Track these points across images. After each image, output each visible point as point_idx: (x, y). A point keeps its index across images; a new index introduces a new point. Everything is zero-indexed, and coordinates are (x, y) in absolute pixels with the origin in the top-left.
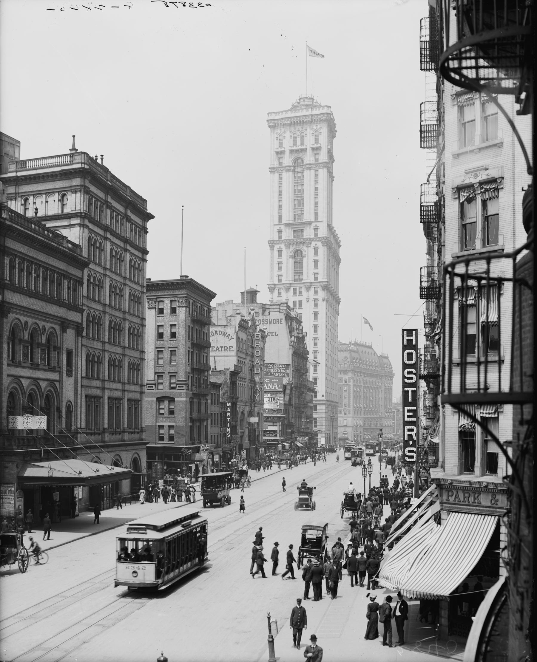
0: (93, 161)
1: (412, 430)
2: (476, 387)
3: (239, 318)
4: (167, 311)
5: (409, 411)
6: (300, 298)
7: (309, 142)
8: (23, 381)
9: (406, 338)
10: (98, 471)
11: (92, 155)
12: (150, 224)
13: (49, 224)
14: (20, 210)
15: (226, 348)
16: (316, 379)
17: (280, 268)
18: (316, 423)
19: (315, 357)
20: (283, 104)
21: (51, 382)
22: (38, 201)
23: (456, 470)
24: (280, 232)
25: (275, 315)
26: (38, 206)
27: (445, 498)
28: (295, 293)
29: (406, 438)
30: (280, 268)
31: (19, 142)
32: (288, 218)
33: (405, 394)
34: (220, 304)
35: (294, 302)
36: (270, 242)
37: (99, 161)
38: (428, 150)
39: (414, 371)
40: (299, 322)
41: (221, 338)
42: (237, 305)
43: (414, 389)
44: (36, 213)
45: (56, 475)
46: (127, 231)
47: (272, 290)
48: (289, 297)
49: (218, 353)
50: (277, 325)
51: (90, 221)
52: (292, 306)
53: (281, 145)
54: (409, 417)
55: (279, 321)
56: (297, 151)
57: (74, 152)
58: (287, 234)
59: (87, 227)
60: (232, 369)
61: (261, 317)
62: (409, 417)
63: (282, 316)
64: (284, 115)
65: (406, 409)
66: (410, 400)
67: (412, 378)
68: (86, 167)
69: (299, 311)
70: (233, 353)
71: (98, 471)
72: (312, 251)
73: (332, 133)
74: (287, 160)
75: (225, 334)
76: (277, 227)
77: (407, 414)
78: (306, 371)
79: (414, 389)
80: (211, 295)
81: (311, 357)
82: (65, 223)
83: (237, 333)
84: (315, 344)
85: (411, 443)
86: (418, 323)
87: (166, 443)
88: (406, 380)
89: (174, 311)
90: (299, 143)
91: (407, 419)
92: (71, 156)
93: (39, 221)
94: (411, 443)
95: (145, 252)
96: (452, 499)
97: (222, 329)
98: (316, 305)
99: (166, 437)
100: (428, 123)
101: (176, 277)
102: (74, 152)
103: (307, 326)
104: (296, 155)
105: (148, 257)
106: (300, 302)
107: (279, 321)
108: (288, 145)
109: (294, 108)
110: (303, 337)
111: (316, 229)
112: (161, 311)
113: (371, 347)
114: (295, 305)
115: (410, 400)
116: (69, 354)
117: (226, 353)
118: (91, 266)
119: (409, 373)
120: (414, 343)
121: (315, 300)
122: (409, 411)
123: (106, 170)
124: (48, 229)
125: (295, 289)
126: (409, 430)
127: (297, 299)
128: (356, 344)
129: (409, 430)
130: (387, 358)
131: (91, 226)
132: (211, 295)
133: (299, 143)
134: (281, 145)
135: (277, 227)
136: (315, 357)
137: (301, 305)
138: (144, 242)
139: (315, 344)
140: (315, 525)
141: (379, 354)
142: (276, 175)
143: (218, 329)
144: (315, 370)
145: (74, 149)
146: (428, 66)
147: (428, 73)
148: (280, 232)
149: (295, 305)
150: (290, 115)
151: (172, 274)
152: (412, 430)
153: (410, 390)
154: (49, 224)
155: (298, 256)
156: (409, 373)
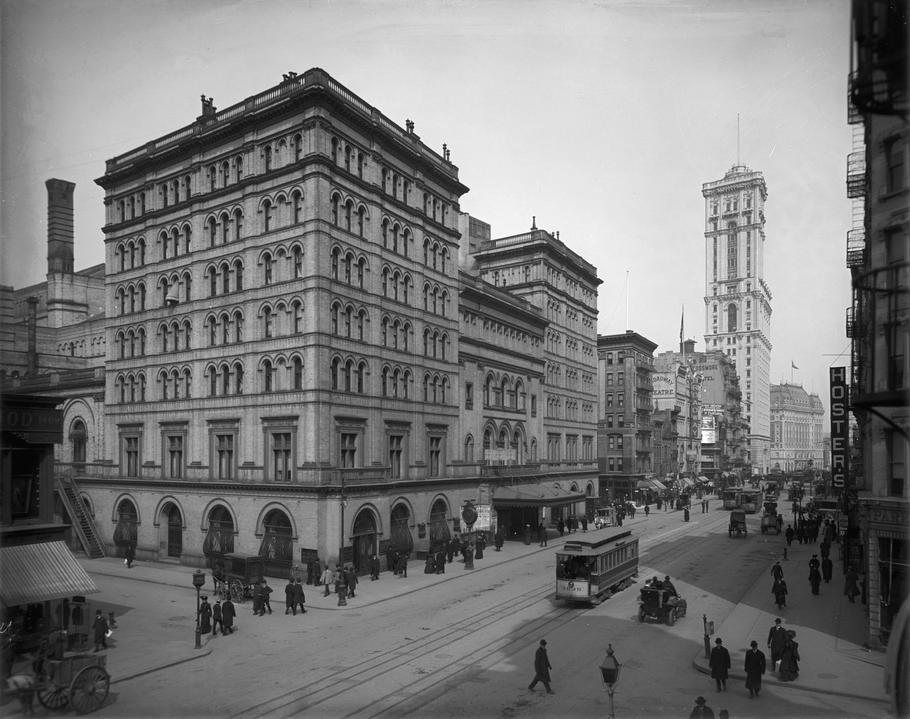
0: (551, 237)
1: (841, 459)
2: (877, 287)
3: (678, 365)
4: (615, 361)
5: (837, 441)
6: (734, 347)
7: (742, 206)
8: (511, 422)
9: (834, 375)
10: (557, 494)
11: (550, 232)
12: (600, 288)
13: (516, 292)
14: (492, 281)
15: (667, 392)
16: (749, 417)
17: (715, 321)
18: (749, 455)
19: (749, 398)
20: (717, 174)
21: (520, 422)
22: (506, 273)
23: (885, 492)
24: (715, 289)
25: (710, 362)
26: (506, 277)
27: (872, 518)
28: (729, 342)
29: (835, 466)
30: (715, 321)
31: (489, 226)
32: (723, 275)
33: (834, 426)
34: (661, 355)
35: (729, 350)
36: (706, 299)
37: (556, 237)
38: (855, 199)
39: (842, 405)
40: (733, 367)
41: (663, 383)
42: (677, 354)
43: (842, 421)
44: (505, 283)
45: (523, 497)
46: (577, 293)
47: (707, 341)
48: (724, 346)
49: (660, 396)
50: (713, 371)
51: (549, 288)
52: (726, 353)
53: (715, 212)
54: (837, 447)
55: (714, 367)
56: (731, 216)
57: (535, 231)
58: (723, 290)
59: (547, 293)
60: (673, 409)
61: (698, 364)
62: (837, 447)
63: (717, 363)
64: (719, 185)
65: (835, 439)
66: (839, 431)
67: (840, 412)
68: (545, 242)
69: (733, 358)
70: (673, 396)
71: (557, 494)
72: (744, 304)
73: (764, 196)
74: (723, 225)
75: (665, 380)
76: (712, 285)
77: (835, 444)
78: (740, 409)
79: (842, 421)
80: (653, 346)
81: (744, 397)
82: (528, 290)
83: (676, 378)
84: (749, 387)
85: (840, 470)
86: (845, 362)
87: (616, 472)
88: (834, 414)
89: (621, 361)
90: (732, 208)
91: (835, 449)
92: (532, 234)
93: (506, 290)
94: (840, 470)
95: (596, 312)
96: (879, 519)
97: (663, 376)
98: (749, 352)
99: (616, 467)
100: (855, 173)
101: (623, 332)
102: (535, 231)
103: (741, 371)
104: (730, 220)
105: (598, 316)
106: (734, 350)
107: (714, 367)
108: (722, 210)
109: (727, 177)
110: (737, 380)
111: (749, 285)
112: (610, 362)
113: (801, 388)
114: (729, 353)
115: (839, 431)
116: (534, 398)
117: (667, 396)
118: (551, 325)
119: (836, 407)
120: (842, 379)
121: (749, 349)
122: (837, 441)
123: (562, 244)
124: (515, 297)
125: (729, 339)
126: (838, 459)
127: (732, 347)
128: (786, 385)
129: (838, 459)
130: (817, 397)
131: (550, 292)
132: (653, 346)
133: (732, 208)
134: (715, 212)
135: (712, 285)
136: (749, 398)
137: (734, 353)
138: (596, 303)
139: (749, 387)
140: (396, 112)
141: (809, 394)
142: (712, 240)
143: (660, 375)
144: (749, 409)
145: (534, 227)
146: (856, 119)
147: (856, 126)
148: (715, 289)
149: (729, 353)
150: (724, 183)
151: (619, 330)
152: (841, 459)
153: (838, 422)
154: (516, 292)
155: (733, 311)
156: (836, 407)
